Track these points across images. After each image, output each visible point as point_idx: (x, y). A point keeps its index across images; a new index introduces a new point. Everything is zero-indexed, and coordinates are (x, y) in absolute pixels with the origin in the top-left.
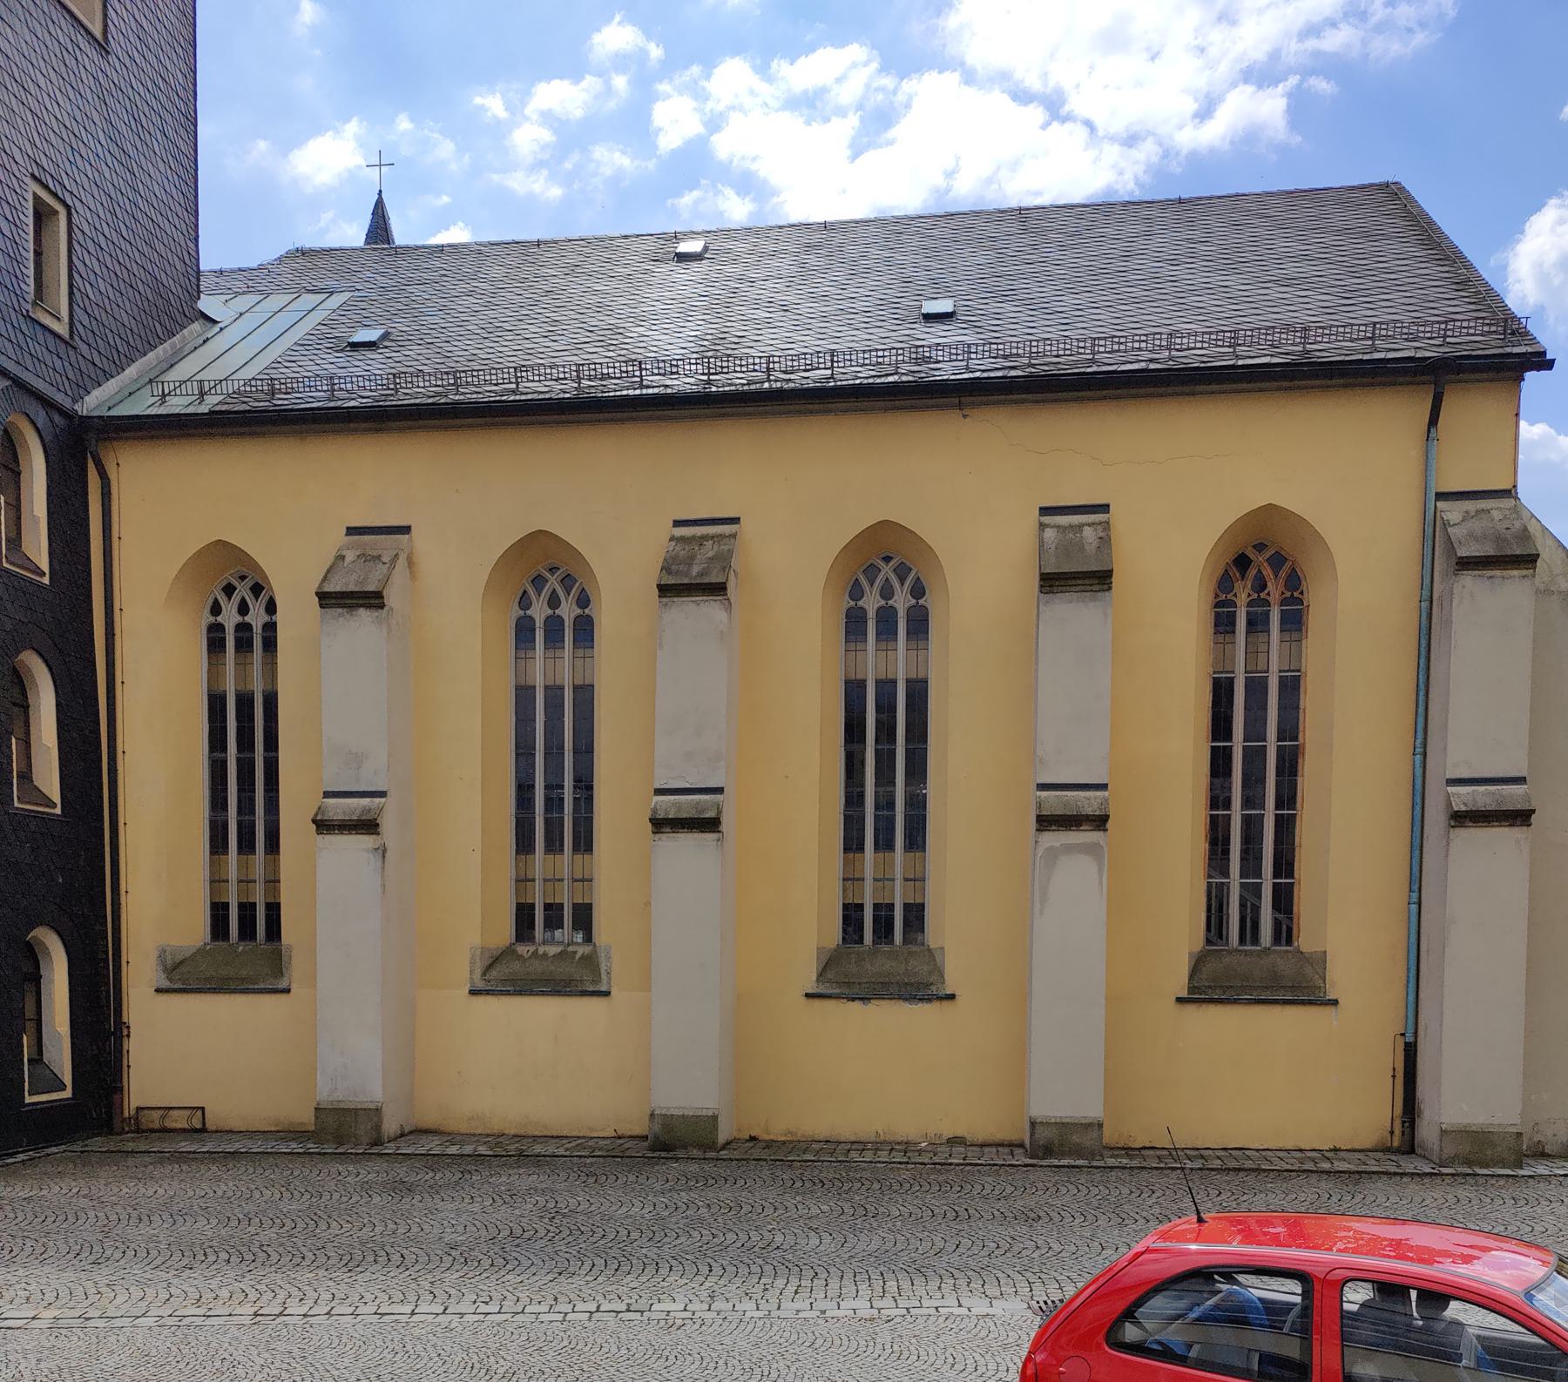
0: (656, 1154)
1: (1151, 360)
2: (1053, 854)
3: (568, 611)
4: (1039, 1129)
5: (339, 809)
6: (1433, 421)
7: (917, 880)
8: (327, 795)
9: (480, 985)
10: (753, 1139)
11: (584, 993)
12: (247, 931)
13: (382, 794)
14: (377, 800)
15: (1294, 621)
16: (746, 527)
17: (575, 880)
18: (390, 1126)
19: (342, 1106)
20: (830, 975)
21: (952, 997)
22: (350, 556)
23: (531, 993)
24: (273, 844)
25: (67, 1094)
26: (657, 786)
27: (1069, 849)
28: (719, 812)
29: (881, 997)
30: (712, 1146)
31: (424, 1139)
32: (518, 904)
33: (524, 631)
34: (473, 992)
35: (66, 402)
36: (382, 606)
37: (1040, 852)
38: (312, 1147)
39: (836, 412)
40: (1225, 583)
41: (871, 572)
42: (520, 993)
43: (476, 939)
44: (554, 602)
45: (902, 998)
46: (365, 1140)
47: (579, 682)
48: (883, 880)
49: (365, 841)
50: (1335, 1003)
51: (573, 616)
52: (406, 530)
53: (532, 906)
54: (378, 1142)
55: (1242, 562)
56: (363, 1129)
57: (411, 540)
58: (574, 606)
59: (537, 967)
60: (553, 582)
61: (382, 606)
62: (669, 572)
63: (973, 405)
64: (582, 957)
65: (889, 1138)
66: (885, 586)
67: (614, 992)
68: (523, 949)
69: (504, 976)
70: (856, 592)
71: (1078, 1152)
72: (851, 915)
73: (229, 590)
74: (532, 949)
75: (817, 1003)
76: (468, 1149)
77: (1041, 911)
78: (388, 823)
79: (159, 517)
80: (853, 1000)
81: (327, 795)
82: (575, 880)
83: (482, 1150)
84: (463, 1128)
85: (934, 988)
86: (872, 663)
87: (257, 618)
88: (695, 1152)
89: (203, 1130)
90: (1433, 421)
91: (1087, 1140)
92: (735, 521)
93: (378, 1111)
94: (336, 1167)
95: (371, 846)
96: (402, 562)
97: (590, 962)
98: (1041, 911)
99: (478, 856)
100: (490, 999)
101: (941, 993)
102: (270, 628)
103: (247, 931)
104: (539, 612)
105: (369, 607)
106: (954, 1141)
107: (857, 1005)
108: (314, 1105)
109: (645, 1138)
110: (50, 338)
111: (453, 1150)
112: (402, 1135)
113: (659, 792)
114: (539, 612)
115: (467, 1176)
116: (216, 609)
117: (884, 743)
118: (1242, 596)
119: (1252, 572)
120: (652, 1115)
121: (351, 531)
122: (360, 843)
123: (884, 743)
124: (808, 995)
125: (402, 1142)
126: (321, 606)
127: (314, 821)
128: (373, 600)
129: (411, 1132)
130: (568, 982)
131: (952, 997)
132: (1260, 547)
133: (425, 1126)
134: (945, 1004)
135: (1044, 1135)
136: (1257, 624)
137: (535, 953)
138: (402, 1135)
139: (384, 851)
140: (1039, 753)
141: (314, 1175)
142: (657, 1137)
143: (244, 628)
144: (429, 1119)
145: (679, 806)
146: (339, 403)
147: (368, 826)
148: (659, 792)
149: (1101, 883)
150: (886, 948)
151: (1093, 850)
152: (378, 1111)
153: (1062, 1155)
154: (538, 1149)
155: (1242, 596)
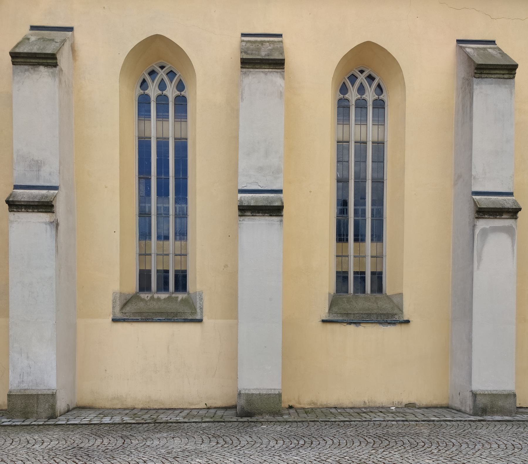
0: (245, 419)
2: (485, 232)
3: (171, 92)
4: (479, 398)
5: (24, 195)
7: (379, 257)
8: (16, 187)
9: (119, 316)
10: (291, 407)
11: (186, 321)
13: (56, 188)
14: (52, 192)
16: (285, 39)
17: (176, 255)
18: (61, 405)
19: (27, 392)
20: (335, 309)
21: (408, 322)
22: (33, 39)
23: (152, 320)
26: (240, 187)
27: (495, 230)
28: (283, 203)
29: (367, 322)
31: (84, 413)
32: (141, 271)
33: (143, 103)
34: (115, 320)
36: (55, 65)
37: (477, 231)
41: (353, 78)
43: (116, 287)
44: (162, 86)
45: (380, 323)
46: (44, 415)
47: (178, 136)
48: (360, 257)
49: (44, 217)
51: (174, 95)
52: (71, 29)
53: (150, 271)
54: (53, 416)
56: (43, 409)
57: (73, 35)
58: (175, 89)
59: (155, 306)
60: (162, 74)
61: (55, 65)
62: (246, 52)
64: (182, 300)
65: (372, 405)
67: (205, 319)
68: (145, 296)
69: (131, 311)
70: (344, 89)
71: (502, 411)
72: (342, 277)
74: (150, 295)
75: (329, 326)
76: (117, 419)
77: (478, 268)
78: (60, 206)
80: (350, 323)
81: (16, 187)
82: (176, 255)
83: (127, 419)
84: (108, 405)
85: (397, 317)
86: (355, 132)
88: (267, 417)
91: (507, 404)
92: (280, 36)
93: (53, 395)
94: (25, 436)
95: (48, 220)
97: (190, 303)
98: (478, 268)
99: (117, 236)
101: (401, 320)
104: (153, 92)
105: (47, 65)
106: (410, 406)
107: (352, 327)
108: (7, 393)
109: (234, 407)
111: (107, 420)
112: (68, 411)
113: (242, 191)
114: (153, 92)
115: (128, 441)
120: (240, 394)
122: (40, 218)
124: (324, 321)
125: (69, 416)
126: (14, 63)
127: (7, 202)
128: (49, 60)
129: (74, 409)
130: (176, 314)
131: (408, 322)
133: (82, 403)
134: (404, 327)
135: (482, 402)
137: (152, 298)
138: (68, 411)
139: (57, 225)
140: (473, 173)
141: (8, 443)
142: (242, 409)
144: (86, 400)
145: (256, 199)
147: (46, 206)
148: (242, 191)
149: (513, 250)
150: (362, 295)
151: (510, 231)
152: (53, 395)
153: (493, 413)
154: (163, 418)
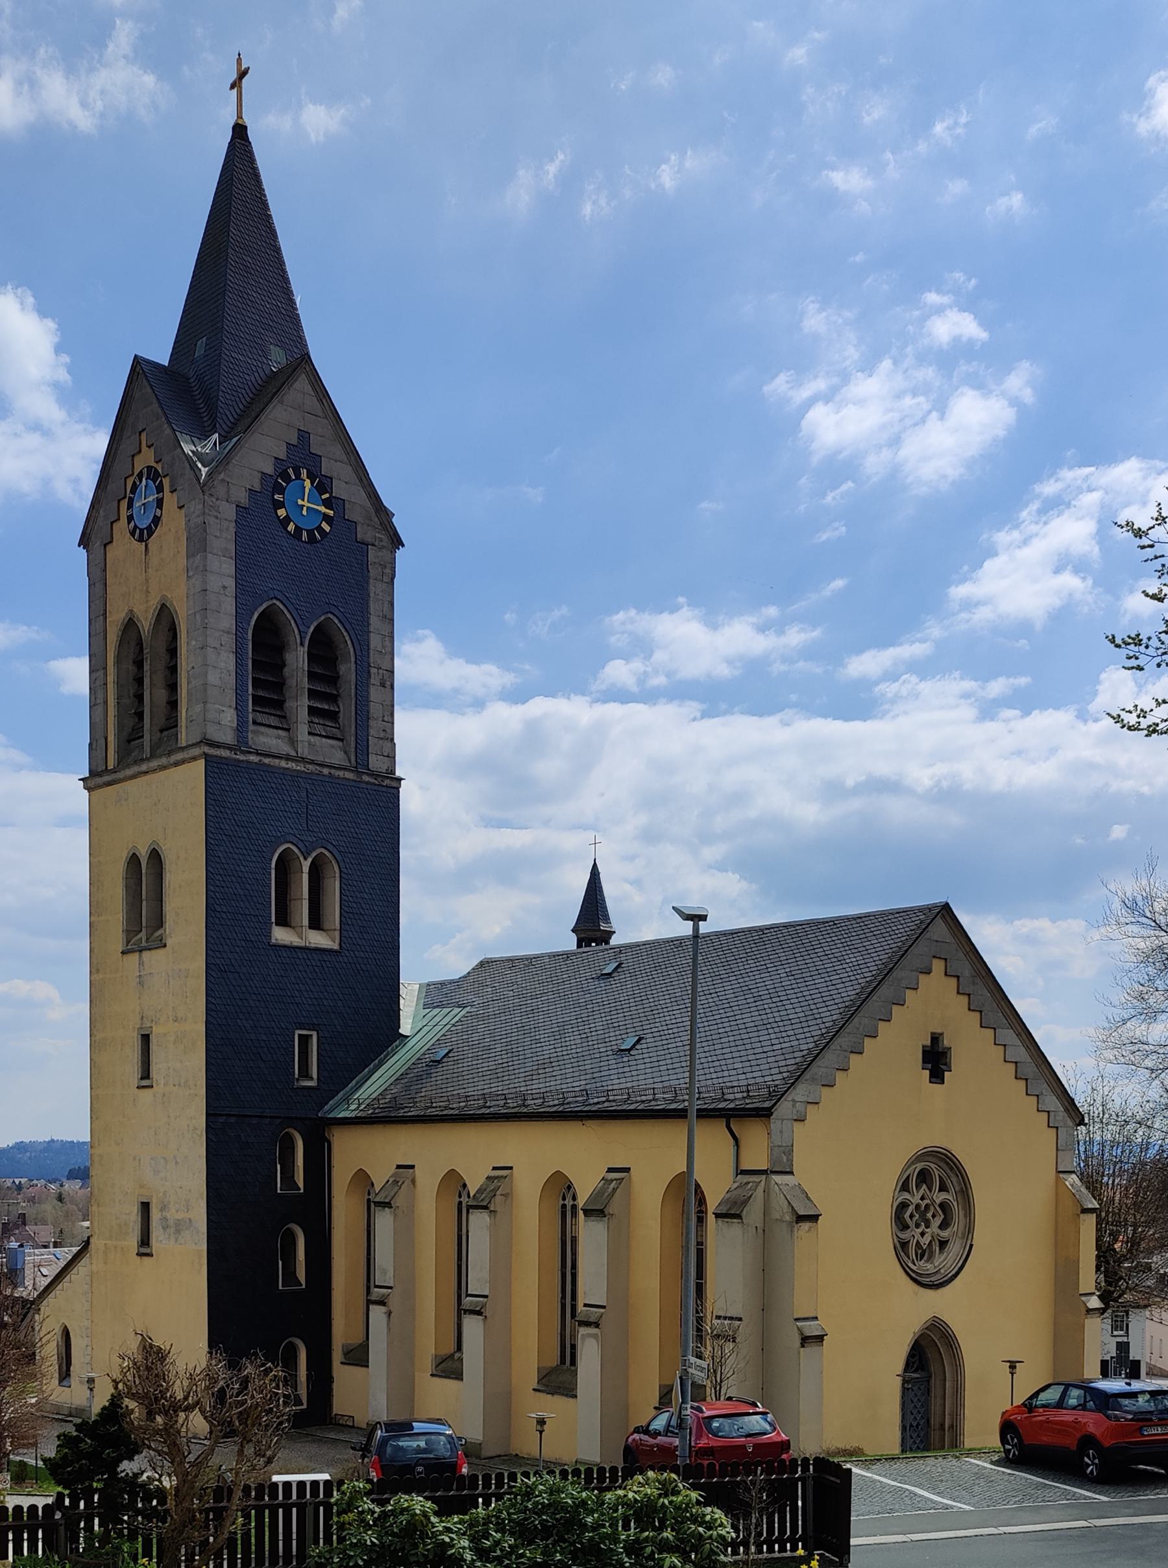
23: (449, 1378)
25: (305, 1407)
30: (479, 1457)
52: (412, 1167)
75: (538, 1394)
121: (398, 1167)
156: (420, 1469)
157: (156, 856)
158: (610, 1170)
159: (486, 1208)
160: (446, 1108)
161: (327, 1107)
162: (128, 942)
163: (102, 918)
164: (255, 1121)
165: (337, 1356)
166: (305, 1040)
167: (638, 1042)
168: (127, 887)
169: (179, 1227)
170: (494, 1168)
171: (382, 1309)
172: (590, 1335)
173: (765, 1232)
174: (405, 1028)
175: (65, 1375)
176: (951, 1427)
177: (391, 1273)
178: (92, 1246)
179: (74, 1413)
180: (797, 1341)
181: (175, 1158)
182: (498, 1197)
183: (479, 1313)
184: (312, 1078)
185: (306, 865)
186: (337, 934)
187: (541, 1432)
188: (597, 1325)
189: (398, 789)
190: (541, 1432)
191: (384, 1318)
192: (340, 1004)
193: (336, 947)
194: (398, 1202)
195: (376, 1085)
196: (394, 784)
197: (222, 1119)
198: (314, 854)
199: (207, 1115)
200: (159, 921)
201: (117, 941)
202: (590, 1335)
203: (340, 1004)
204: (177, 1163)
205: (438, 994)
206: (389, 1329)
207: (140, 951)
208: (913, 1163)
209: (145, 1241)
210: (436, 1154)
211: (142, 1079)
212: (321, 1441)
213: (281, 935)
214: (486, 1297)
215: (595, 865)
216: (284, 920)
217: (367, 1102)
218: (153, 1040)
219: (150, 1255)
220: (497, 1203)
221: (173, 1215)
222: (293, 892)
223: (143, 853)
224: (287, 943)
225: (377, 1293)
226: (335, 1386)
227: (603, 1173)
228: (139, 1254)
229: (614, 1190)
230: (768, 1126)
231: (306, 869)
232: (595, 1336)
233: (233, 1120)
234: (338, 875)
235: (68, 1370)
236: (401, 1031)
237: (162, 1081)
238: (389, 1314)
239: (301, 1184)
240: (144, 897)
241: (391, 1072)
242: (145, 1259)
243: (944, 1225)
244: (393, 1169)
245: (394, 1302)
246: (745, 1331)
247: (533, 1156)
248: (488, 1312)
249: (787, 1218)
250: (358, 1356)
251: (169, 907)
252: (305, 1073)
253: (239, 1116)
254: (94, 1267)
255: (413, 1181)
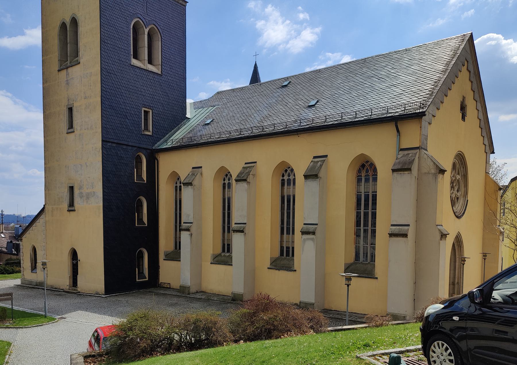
1: (395, 113)
6: (398, 131)
9: (212, 262)
12: (288, 255)
15: (375, 179)
20: (273, 264)
23: (220, 264)
24: (293, 233)
25: (147, 279)
29: (282, 269)
30: (242, 301)
35: (150, 147)
38: (178, 294)
39: (199, 148)
40: (359, 171)
42: (218, 264)
50: (377, 278)
52: (201, 167)
55: (363, 166)
63: (300, 134)
66: (365, 169)
68: (223, 254)
73: (286, 171)
75: (270, 270)
79: (169, 165)
87: (291, 177)
89: (170, 288)
90: (398, 131)
92: (256, 162)
93: (189, 287)
96: (199, 174)
100: (214, 265)
102: (294, 179)
103: (288, 255)
110: (147, 137)
112: (197, 292)
116: (283, 176)
117: (365, 210)
118: (363, 174)
119: (365, 168)
121: (193, 168)
123: (365, 210)
131: (295, 271)
132: (367, 162)
136: (367, 180)
138: (197, 292)
143: (289, 180)
146: (359, 119)
155: (363, 174)
156: (456, 318)
157: (74, 22)
158: (315, 157)
159: (245, 180)
160: (219, 138)
161: (156, 145)
162: (61, 65)
163: (49, 56)
164: (125, 147)
165: (162, 256)
166: (146, 113)
167: (318, 102)
168: (60, 39)
169: (88, 197)
170: (246, 163)
171: (187, 233)
172: (308, 239)
173: (419, 179)
174: (188, 115)
175: (34, 268)
176: (458, 283)
177: (191, 216)
178: (46, 209)
179: (38, 284)
180: (438, 236)
181: (86, 163)
182: (251, 176)
183: (242, 231)
184: (150, 132)
185: (146, 31)
186: (160, 67)
187: (348, 286)
188: (314, 233)
189: (185, 6)
190: (348, 286)
191: (189, 237)
192: (161, 99)
193: (160, 73)
194: (195, 183)
195: (179, 135)
196: (184, 3)
197: (109, 144)
198: (150, 27)
199: (103, 141)
200: (76, 53)
201: (55, 65)
202: (308, 239)
203: (161, 99)
204: (87, 166)
205: (200, 105)
206: (191, 242)
207: (67, 68)
208: (24, 315)
209: (71, 204)
210: (210, 161)
211: (69, 129)
212: (157, 294)
213: (134, 62)
214: (245, 224)
215: (256, 64)
216: (136, 57)
217: (177, 141)
218: (74, 110)
219: (74, 210)
220: (250, 179)
221: (85, 191)
222: (140, 44)
223: (68, 21)
224: (139, 66)
225: (184, 226)
226: (160, 270)
227: (311, 159)
228: (69, 211)
229: (321, 166)
230: (421, 123)
231: (146, 33)
232: (312, 239)
233: (114, 145)
234: (160, 39)
235: (35, 265)
236: (187, 116)
237: (79, 128)
238: (191, 235)
239: (145, 179)
240: (68, 42)
241: (185, 130)
242: (71, 212)
243: (458, 191)
244: (191, 169)
245: (193, 229)
246: (411, 232)
247: (267, 157)
248: (246, 231)
249: (433, 171)
250: (175, 255)
251: (81, 44)
252: (146, 128)
253: (117, 143)
254: (47, 219)
255: (201, 174)
